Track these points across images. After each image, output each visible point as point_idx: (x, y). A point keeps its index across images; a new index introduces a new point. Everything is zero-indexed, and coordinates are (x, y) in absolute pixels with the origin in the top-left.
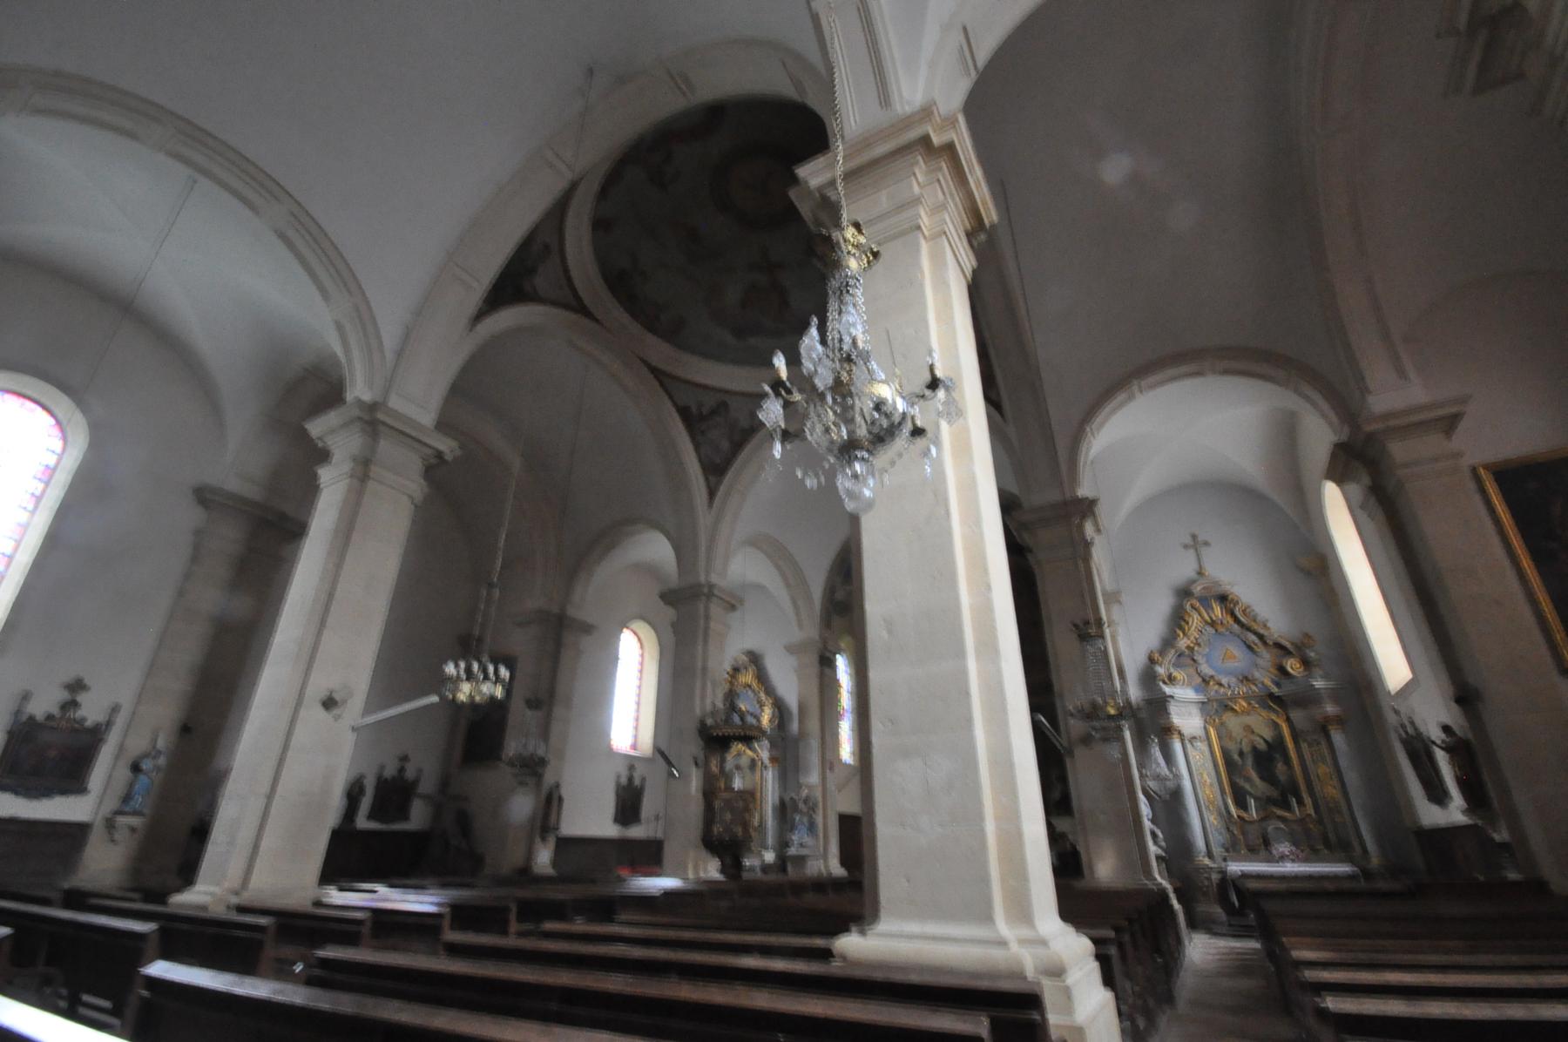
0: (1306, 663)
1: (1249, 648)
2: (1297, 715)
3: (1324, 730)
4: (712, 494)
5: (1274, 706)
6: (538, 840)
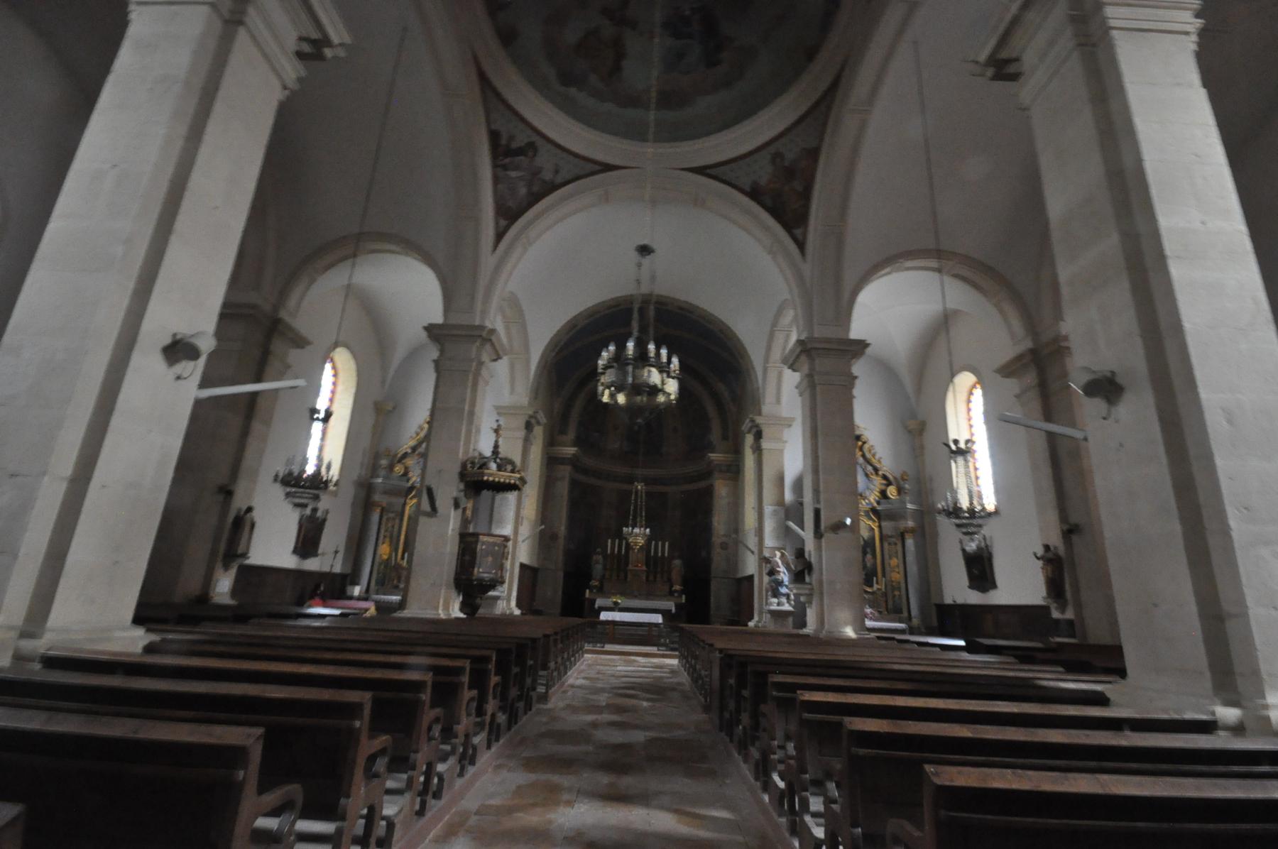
0: (900, 490)
3: (902, 536)
4: (499, 236)
5: (873, 517)
6: (219, 565)
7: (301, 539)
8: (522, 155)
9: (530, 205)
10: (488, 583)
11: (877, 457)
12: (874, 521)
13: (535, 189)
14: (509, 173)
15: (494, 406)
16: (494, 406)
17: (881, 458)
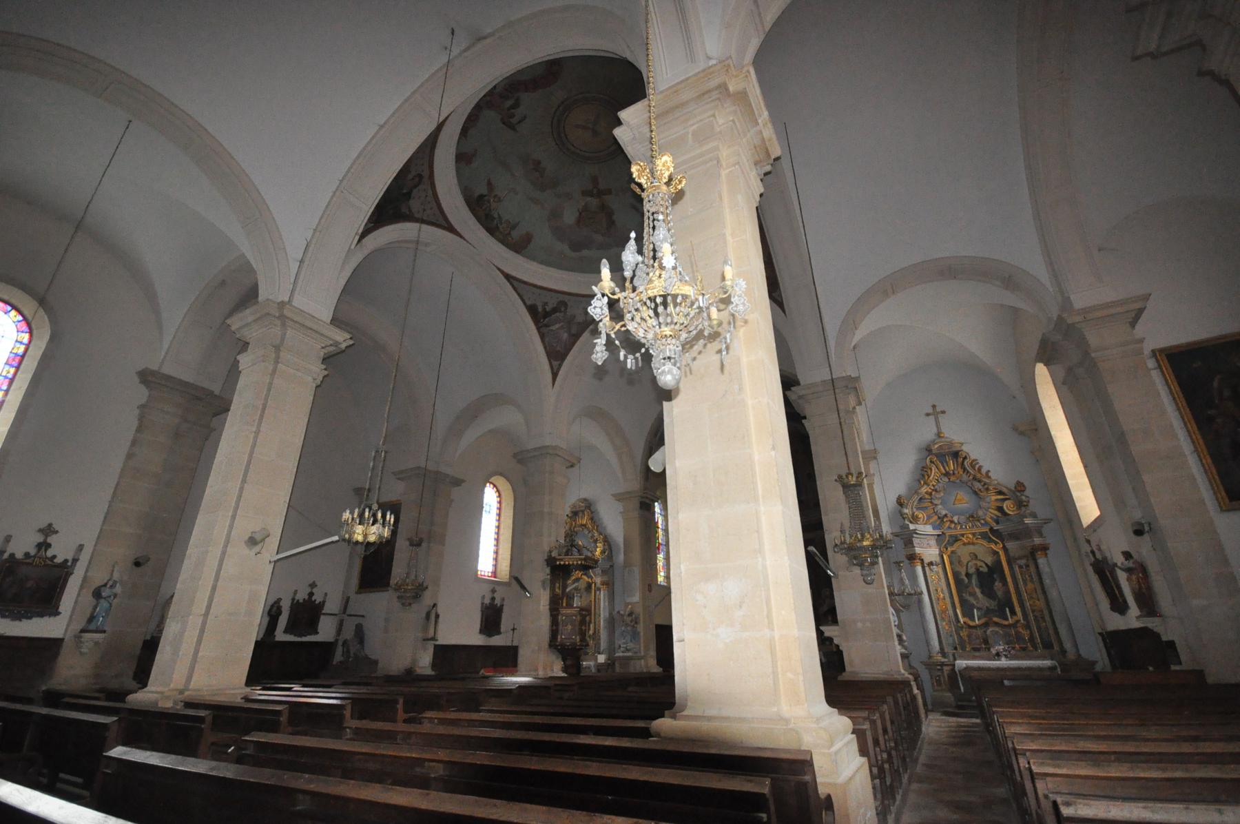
1: (975, 493)
2: (1011, 545)
7: (484, 619)
8: (556, 312)
9: (573, 344)
10: (570, 647)
11: (984, 471)
12: (996, 543)
13: (574, 331)
14: (551, 328)
15: (613, 495)
16: (613, 495)
17: (989, 471)
